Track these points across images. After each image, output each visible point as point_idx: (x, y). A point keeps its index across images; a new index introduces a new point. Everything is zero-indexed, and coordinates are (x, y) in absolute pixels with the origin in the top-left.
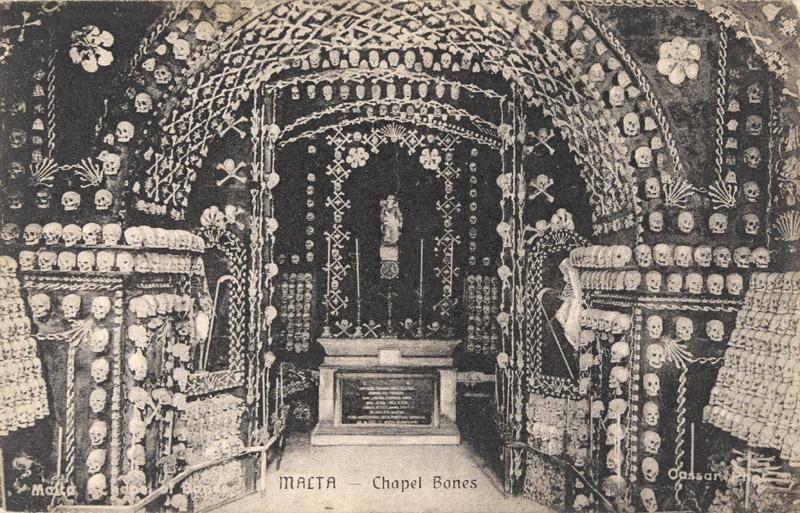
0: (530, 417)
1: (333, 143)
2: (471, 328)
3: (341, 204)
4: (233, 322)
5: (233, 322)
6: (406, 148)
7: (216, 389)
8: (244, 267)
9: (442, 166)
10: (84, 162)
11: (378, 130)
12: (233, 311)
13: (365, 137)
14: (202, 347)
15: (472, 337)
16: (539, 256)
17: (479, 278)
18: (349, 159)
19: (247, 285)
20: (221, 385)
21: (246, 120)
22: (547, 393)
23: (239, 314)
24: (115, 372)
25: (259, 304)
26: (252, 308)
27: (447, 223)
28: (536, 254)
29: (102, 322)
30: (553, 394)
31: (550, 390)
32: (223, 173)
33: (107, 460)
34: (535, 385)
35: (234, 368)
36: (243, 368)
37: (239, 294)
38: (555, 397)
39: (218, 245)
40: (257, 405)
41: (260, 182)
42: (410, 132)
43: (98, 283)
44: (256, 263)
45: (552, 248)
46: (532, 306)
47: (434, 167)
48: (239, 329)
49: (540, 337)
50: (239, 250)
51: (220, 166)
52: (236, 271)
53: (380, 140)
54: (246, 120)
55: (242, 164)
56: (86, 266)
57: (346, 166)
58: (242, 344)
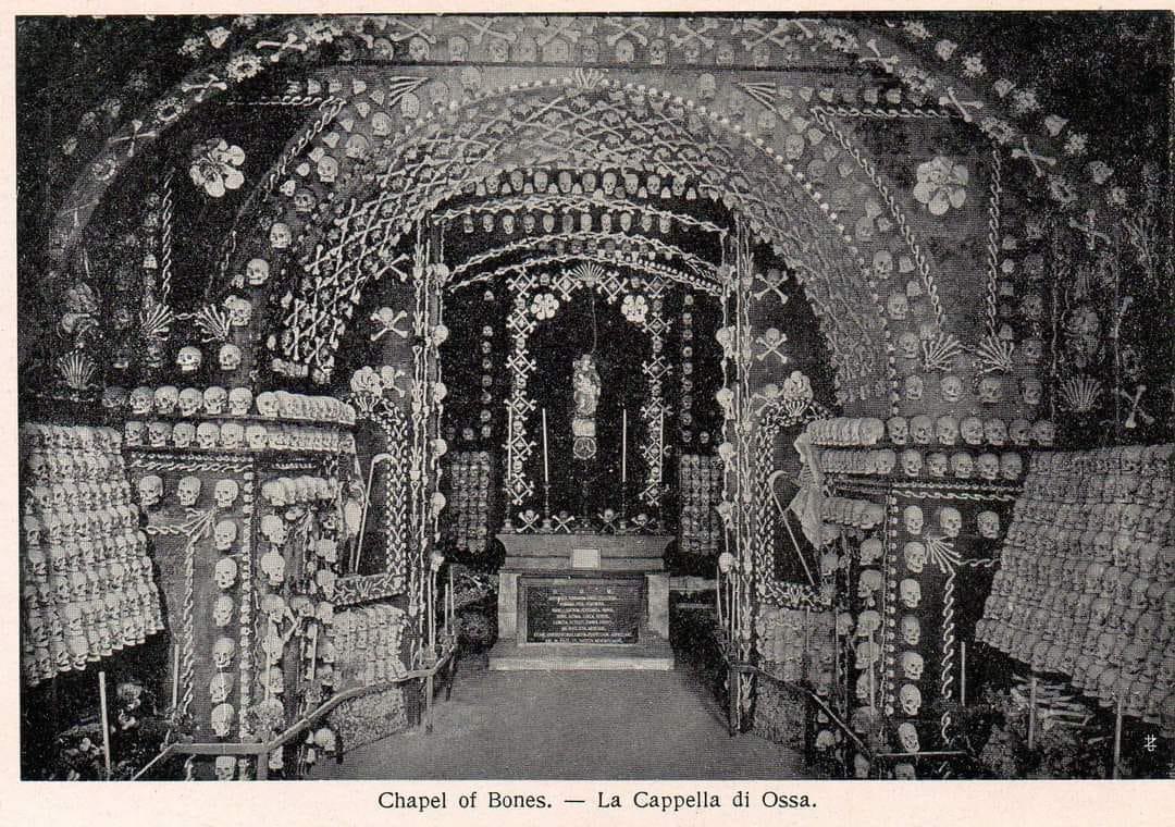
5: (392, 513)
6: (605, 295)
8: (405, 443)
16: (769, 430)
18: (534, 309)
19: (409, 466)
26: (414, 495)
28: (766, 428)
35: (393, 570)
36: (404, 571)
38: (792, 608)
39: (373, 416)
40: (422, 618)
41: (424, 337)
42: (609, 274)
48: (398, 520)
49: (772, 532)
50: (398, 422)
53: (572, 285)
55: (403, 314)
56: (207, 441)
57: (531, 318)
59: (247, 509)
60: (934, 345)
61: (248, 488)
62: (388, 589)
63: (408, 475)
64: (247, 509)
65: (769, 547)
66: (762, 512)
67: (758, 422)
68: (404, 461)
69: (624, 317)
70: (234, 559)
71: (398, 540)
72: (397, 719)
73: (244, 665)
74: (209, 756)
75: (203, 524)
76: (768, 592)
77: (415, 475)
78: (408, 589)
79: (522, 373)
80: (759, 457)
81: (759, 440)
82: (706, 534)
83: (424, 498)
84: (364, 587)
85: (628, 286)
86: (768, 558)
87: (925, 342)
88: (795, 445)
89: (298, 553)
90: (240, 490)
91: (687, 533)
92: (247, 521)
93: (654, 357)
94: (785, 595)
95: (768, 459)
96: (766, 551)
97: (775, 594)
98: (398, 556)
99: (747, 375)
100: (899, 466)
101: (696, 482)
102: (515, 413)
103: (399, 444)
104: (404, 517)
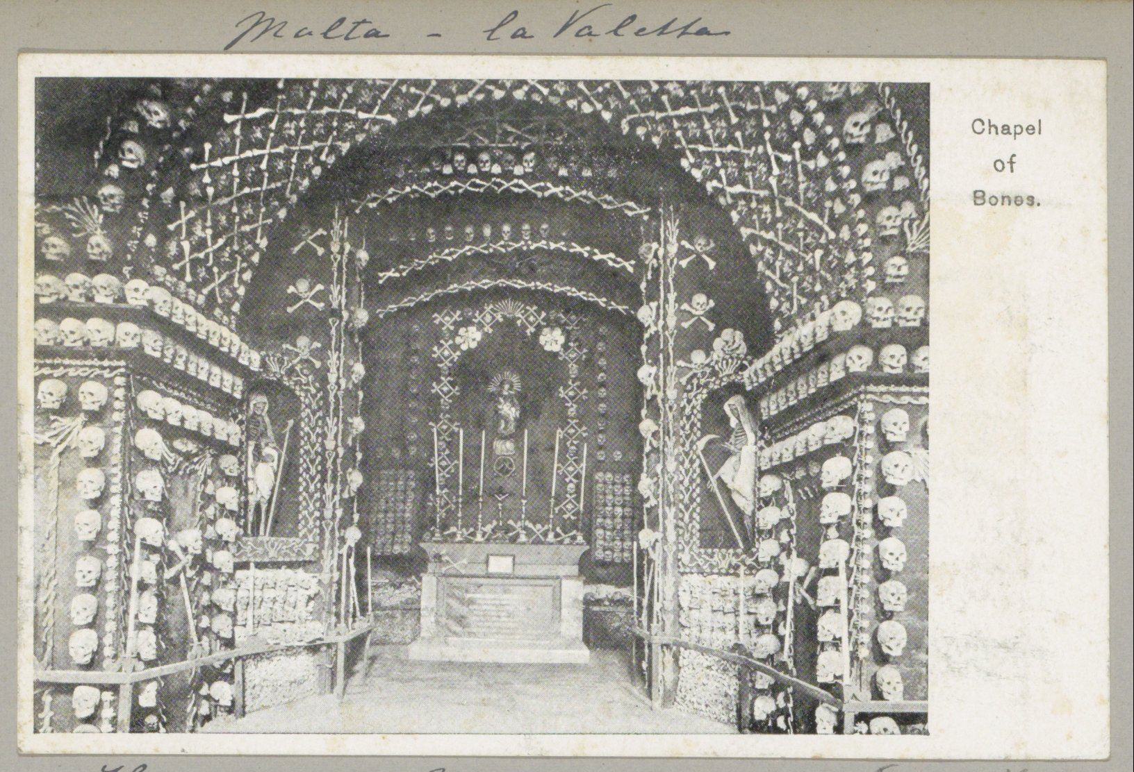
0: (685, 604)
1: (441, 323)
2: (600, 532)
3: (450, 391)
4: (305, 480)
5: (305, 480)
6: (524, 327)
7: (281, 559)
8: (320, 414)
9: (566, 347)
10: (78, 203)
11: (491, 306)
12: (305, 466)
13: (477, 315)
14: (264, 507)
15: (601, 542)
16: (695, 396)
17: (609, 475)
18: (458, 340)
19: (324, 436)
20: (286, 554)
21: (325, 233)
22: (708, 570)
23: (313, 471)
24: (114, 489)
25: (339, 461)
26: (329, 464)
27: (572, 411)
28: (692, 394)
29: (95, 417)
30: (716, 570)
31: (711, 566)
32: (296, 298)
33: (100, 609)
34: (691, 562)
35: (305, 536)
36: (318, 538)
37: (313, 446)
38: (719, 574)
39: (285, 379)
40: (335, 587)
41: (341, 310)
42: (528, 308)
43: (91, 367)
44: (335, 409)
45: (714, 382)
46: (687, 462)
47: (556, 348)
48: (312, 488)
49: (698, 500)
50: (313, 391)
51: (291, 289)
52: (308, 416)
53: (494, 318)
54: (325, 233)
55: (320, 287)
56: (72, 337)
57: (455, 347)
58: (316, 509)
59: (117, 417)
60: (918, 227)
61: (120, 393)
62: (299, 553)
63: (323, 445)
64: (117, 417)
65: (695, 515)
66: (686, 482)
67: (683, 389)
68: (318, 430)
69: (542, 347)
70: (103, 471)
71: (311, 508)
72: (307, 685)
73: (111, 587)
74: (68, 685)
75: (69, 433)
76: (692, 559)
77: (330, 444)
78: (321, 557)
79: (446, 398)
80: (684, 425)
81: (684, 408)
82: (619, 543)
83: (339, 469)
84: (269, 545)
85: (546, 319)
86: (693, 527)
87: (907, 223)
88: (726, 408)
89: (191, 493)
90: (110, 395)
91: (600, 542)
92: (118, 430)
93: (570, 383)
94: (713, 561)
95: (695, 425)
96: (691, 518)
97: (700, 562)
98: (311, 523)
99: (671, 342)
100: (877, 364)
101: (610, 497)
102: (439, 434)
103: (314, 413)
104: (319, 485)
